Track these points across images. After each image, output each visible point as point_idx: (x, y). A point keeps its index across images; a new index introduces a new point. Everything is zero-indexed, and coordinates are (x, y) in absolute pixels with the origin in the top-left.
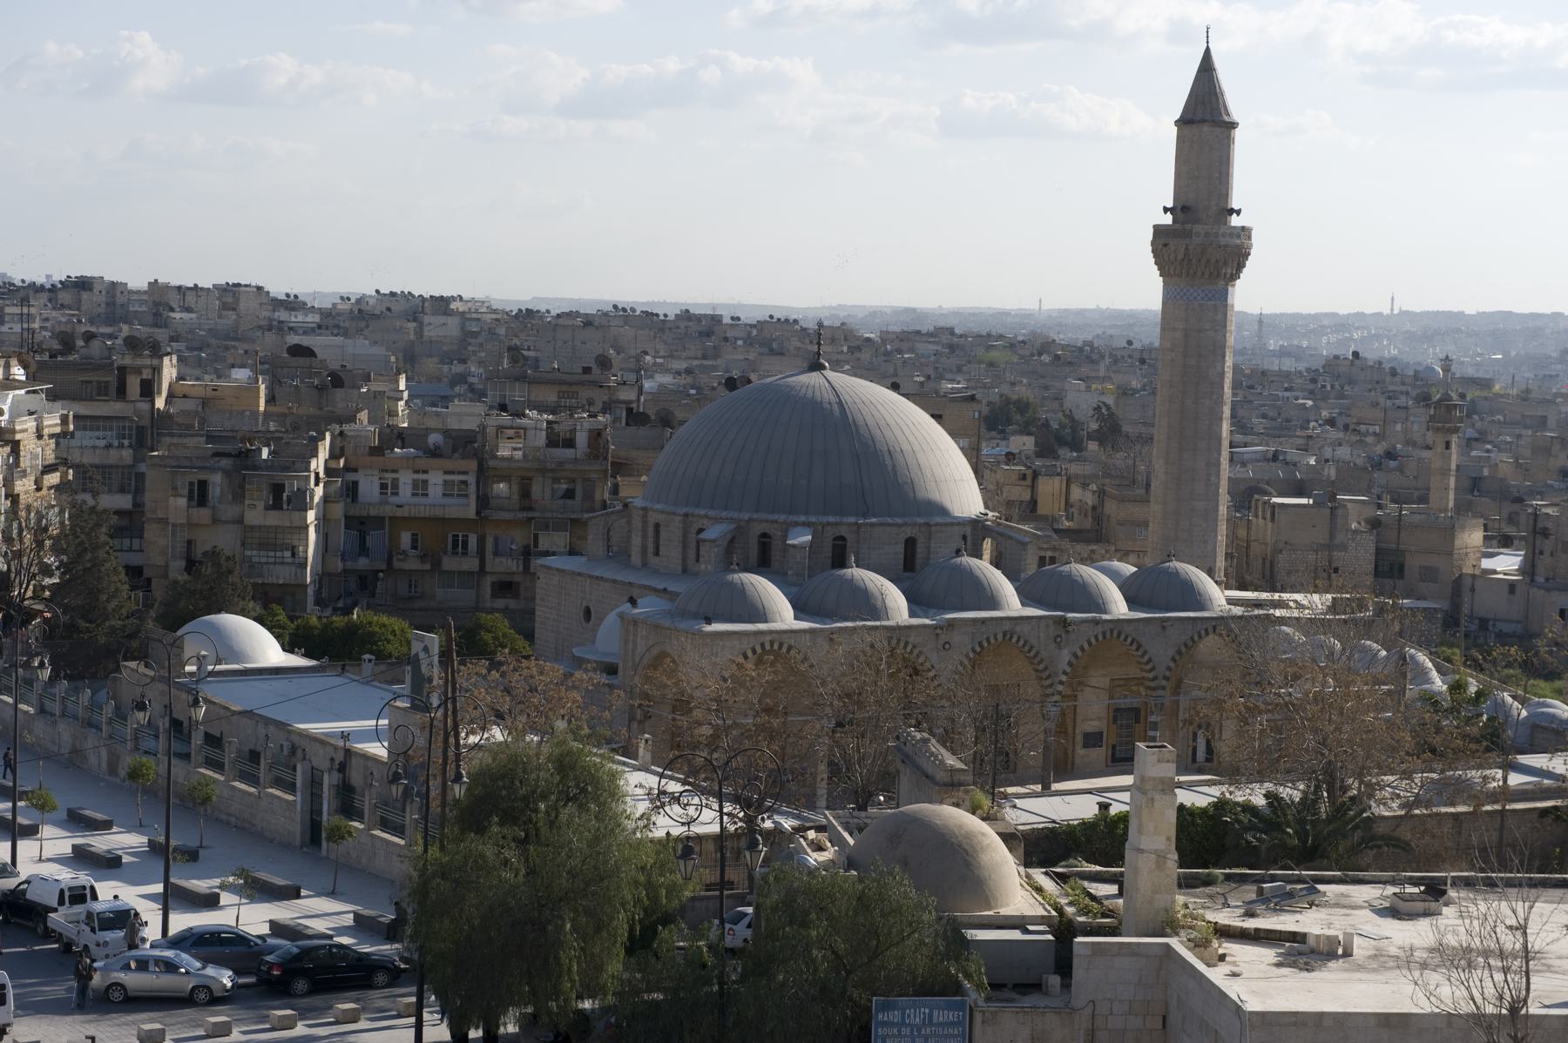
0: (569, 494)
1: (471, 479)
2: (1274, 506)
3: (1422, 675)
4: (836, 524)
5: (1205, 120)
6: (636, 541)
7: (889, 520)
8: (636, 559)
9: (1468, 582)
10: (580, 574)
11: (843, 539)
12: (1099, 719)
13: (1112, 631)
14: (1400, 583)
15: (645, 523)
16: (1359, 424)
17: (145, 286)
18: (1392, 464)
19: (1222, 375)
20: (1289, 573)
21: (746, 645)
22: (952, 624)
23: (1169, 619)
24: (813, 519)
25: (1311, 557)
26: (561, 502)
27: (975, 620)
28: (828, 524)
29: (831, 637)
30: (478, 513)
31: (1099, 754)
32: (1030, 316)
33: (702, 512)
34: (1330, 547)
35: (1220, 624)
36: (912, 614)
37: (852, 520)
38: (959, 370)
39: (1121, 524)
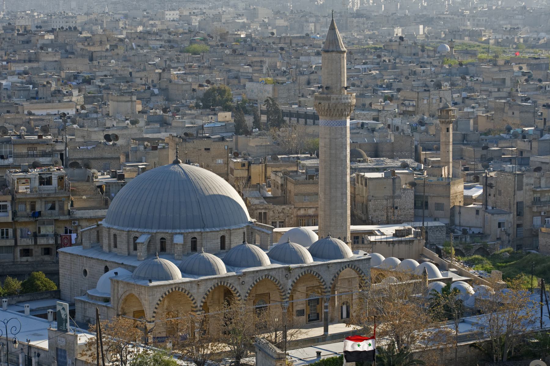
0: (53, 208)
1: (9, 204)
2: (366, 179)
3: (434, 274)
4: (192, 232)
7: (214, 229)
8: (106, 248)
9: (457, 209)
10: (81, 256)
11: (195, 238)
12: (303, 304)
13: (308, 271)
14: (426, 212)
15: (109, 234)
16: (405, 100)
18: (423, 128)
19: (346, 156)
20: (375, 211)
21: (165, 290)
22: (245, 274)
23: (330, 263)
24: (183, 231)
25: (385, 202)
26: (50, 212)
27: (253, 272)
28: (189, 233)
29: (198, 283)
30: (13, 219)
31: (303, 319)
33: (136, 230)
34: (393, 197)
35: (352, 264)
36: (228, 271)
37: (199, 230)
39: (296, 195)
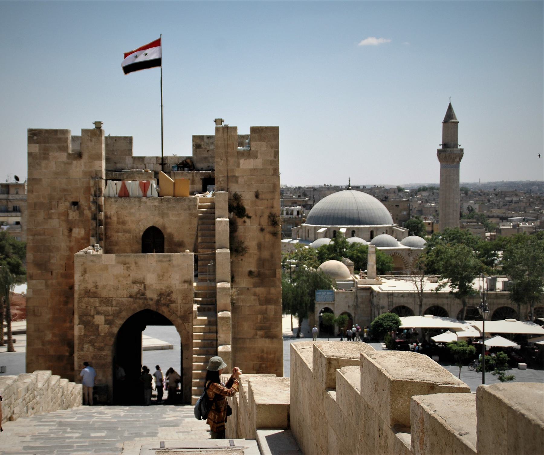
5: (450, 122)
17: (204, 422)
32: (475, 184)
38: (434, 200)
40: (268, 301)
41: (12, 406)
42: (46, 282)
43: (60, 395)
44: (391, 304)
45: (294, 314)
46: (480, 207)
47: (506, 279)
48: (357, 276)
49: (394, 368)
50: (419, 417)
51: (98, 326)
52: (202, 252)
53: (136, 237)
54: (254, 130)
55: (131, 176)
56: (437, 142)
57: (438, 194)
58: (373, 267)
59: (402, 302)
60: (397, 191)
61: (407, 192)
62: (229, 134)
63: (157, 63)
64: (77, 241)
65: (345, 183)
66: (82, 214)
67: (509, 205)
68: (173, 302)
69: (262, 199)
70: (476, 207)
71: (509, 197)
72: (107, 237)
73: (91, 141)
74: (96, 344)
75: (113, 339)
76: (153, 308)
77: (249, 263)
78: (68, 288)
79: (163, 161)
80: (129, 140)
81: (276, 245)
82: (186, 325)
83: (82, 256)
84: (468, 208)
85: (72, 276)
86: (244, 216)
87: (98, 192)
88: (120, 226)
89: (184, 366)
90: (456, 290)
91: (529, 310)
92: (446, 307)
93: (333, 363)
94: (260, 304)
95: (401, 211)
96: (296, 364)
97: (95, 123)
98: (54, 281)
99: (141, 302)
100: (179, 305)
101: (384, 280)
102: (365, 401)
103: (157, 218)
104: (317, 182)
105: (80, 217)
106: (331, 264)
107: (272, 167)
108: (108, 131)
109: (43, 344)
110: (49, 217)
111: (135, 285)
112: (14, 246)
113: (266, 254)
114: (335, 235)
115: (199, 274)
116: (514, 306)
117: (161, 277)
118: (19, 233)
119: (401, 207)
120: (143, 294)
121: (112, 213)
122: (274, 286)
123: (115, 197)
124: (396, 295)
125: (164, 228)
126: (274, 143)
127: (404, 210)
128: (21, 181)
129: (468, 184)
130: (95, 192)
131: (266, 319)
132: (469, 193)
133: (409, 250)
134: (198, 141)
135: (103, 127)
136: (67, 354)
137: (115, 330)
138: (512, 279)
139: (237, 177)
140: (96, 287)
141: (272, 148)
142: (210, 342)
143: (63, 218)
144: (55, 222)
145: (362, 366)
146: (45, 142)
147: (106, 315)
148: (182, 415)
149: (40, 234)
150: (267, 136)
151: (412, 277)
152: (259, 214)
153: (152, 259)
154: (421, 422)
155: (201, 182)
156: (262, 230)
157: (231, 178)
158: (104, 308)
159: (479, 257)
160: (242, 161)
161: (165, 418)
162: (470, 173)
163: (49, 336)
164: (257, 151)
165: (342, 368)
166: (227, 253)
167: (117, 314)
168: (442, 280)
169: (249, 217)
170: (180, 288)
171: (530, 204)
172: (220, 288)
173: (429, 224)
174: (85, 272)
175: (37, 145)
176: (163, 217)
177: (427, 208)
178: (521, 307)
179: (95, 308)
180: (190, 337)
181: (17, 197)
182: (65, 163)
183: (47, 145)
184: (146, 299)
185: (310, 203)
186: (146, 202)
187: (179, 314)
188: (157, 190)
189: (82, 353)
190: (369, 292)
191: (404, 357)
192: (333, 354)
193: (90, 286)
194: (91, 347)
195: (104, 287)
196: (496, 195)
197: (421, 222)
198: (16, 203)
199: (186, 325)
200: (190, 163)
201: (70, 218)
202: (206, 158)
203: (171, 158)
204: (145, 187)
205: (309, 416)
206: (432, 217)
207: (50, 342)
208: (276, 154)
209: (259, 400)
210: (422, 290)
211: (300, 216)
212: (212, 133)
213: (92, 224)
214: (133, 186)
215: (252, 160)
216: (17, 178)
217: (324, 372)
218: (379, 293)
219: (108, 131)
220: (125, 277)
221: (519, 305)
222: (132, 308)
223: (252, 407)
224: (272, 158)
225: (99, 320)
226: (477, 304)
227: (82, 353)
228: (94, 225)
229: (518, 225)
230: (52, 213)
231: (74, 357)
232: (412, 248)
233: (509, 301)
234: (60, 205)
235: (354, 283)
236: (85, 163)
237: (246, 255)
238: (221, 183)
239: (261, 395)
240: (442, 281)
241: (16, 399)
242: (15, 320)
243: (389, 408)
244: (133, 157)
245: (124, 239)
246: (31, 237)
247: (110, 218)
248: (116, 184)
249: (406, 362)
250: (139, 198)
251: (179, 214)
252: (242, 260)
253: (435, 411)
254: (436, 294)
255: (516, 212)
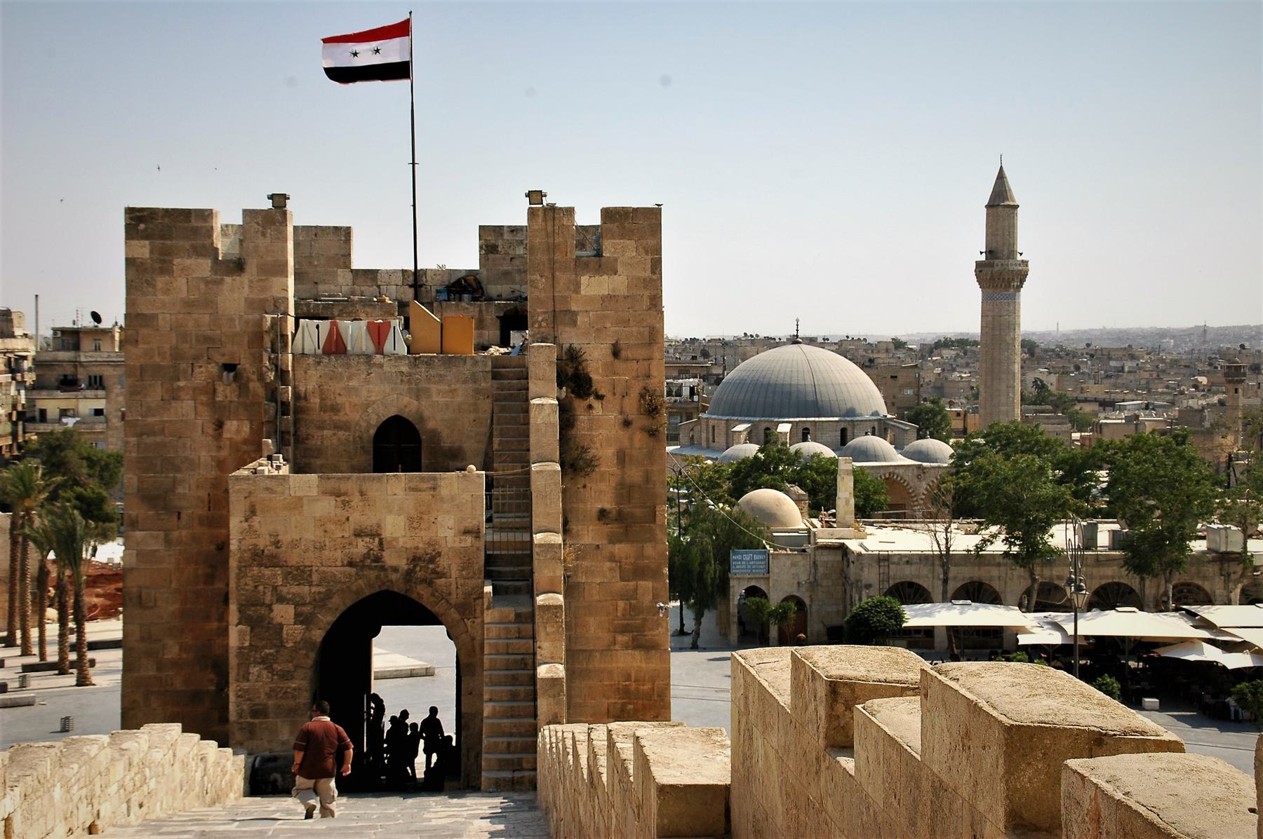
5: (1001, 206)
6: (704, 435)
8: (704, 444)
32: (1050, 334)
38: (967, 365)
40: (639, 572)
41: (95, 801)
42: (166, 535)
43: (198, 775)
44: (885, 577)
45: (687, 600)
46: (1059, 381)
47: (1116, 527)
48: (815, 521)
49: (1007, 699)
50: (1086, 805)
51: (281, 626)
52: (500, 472)
53: (361, 438)
54: (607, 214)
55: (348, 308)
56: (975, 246)
57: (974, 352)
58: (847, 502)
59: (908, 573)
60: (892, 347)
61: (911, 349)
62: (557, 222)
63: (400, 71)
64: (234, 446)
65: (785, 331)
66: (243, 388)
67: (1118, 377)
68: (441, 575)
69: (627, 360)
70: (1051, 381)
71: (1116, 360)
72: (299, 440)
73: (264, 234)
74: (275, 666)
75: (312, 655)
76: (399, 588)
77: (600, 494)
78: (213, 547)
79: (416, 279)
80: (345, 234)
81: (653, 455)
82: (469, 623)
83: (247, 478)
84: (1035, 382)
85: (221, 522)
86: (589, 395)
87: (280, 341)
88: (326, 416)
89: (463, 710)
90: (1015, 549)
91: (1162, 590)
92: (997, 585)
93: (843, 695)
94: (622, 579)
95: (901, 388)
96: (746, 698)
97: (271, 197)
98: (184, 533)
99: (373, 574)
100: (453, 580)
101: (869, 529)
102: (933, 774)
103: (406, 399)
104: (730, 331)
105: (239, 396)
106: (765, 496)
107: (647, 293)
108: (300, 215)
109: (160, 666)
110: (174, 395)
111: (360, 540)
112: (91, 462)
113: (634, 474)
114: (766, 438)
115: (495, 515)
116: (1133, 581)
117: (414, 522)
118: (101, 433)
119: (901, 380)
120: (378, 559)
121: (310, 387)
122: (653, 539)
123: (315, 355)
124: (896, 560)
125: (422, 419)
126: (651, 242)
127: (908, 386)
128: (106, 324)
129: (1034, 334)
130: (273, 344)
131: (634, 610)
132: (1037, 351)
133: (919, 467)
134: (492, 239)
135: (290, 206)
136: (213, 688)
137: (318, 635)
138: (1129, 526)
139: (574, 314)
140: (277, 544)
141: (647, 253)
142: (520, 657)
143: (204, 398)
144: (186, 407)
145: (926, 695)
146: (163, 237)
147: (297, 602)
148: (465, 814)
149: (154, 434)
150: (637, 226)
151: (926, 523)
152: (619, 390)
153: (396, 484)
154: (1092, 819)
155: (498, 322)
156: (627, 424)
157: (561, 316)
158: (295, 589)
159: (1060, 482)
160: (584, 279)
161: (430, 820)
162: (1041, 313)
163: (172, 650)
164: (616, 260)
165: (869, 703)
166: (555, 471)
167: (321, 602)
168: (986, 528)
169: (600, 397)
170: (457, 545)
171: (1160, 373)
172: (541, 546)
173: (958, 414)
174: (253, 512)
175: (147, 242)
176: (418, 398)
177: (953, 381)
178: (1147, 583)
179: (275, 588)
180: (478, 649)
181: (98, 357)
182: (207, 282)
183: (169, 242)
184: (383, 568)
185: (717, 371)
186: (381, 366)
187: (453, 601)
188: (406, 341)
189: (245, 685)
190: (839, 553)
191: (1022, 675)
192: (842, 673)
193: (263, 542)
194: (265, 672)
195: (295, 544)
196: (1092, 356)
197: (942, 409)
198: (95, 371)
199: (469, 623)
200: (474, 284)
201: (219, 398)
202: (506, 274)
203: (435, 272)
204: (378, 334)
205: (780, 809)
206: (964, 401)
207: (175, 664)
208: (657, 265)
209: (665, 775)
210: (948, 549)
211: (696, 398)
212: (522, 220)
213: (266, 412)
214: (354, 331)
215: (605, 277)
216: (96, 317)
217: (822, 712)
218: (860, 554)
219: (300, 215)
220: (339, 523)
221: (1142, 579)
222: (354, 588)
223: (645, 790)
224: (648, 274)
225: (284, 613)
226: (1060, 578)
227: (245, 685)
228: (272, 412)
229: (1137, 417)
230: (180, 388)
231: (228, 696)
232: (925, 464)
233: (1124, 571)
234: (197, 370)
235: (810, 535)
236: (251, 282)
237: (593, 475)
238: (540, 326)
239: (667, 766)
240: (987, 532)
241: (104, 787)
242: (92, 619)
243: (1000, 787)
244: (352, 271)
245: (335, 441)
246: (133, 440)
247: (305, 398)
248: (318, 327)
249: (1031, 687)
250: (368, 357)
251: (453, 391)
252: (585, 486)
253: (1127, 794)
254: (977, 557)
255: (1132, 391)
